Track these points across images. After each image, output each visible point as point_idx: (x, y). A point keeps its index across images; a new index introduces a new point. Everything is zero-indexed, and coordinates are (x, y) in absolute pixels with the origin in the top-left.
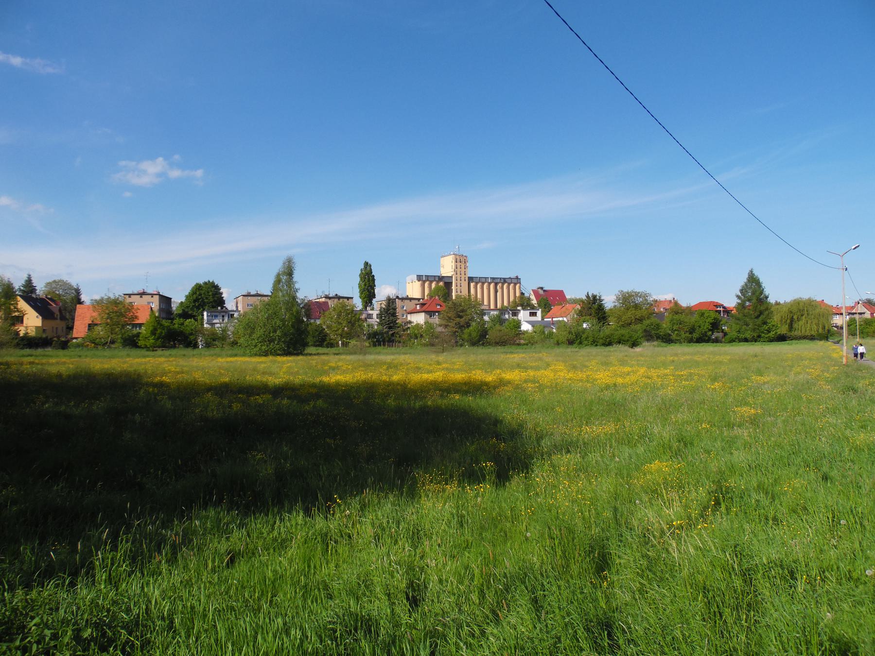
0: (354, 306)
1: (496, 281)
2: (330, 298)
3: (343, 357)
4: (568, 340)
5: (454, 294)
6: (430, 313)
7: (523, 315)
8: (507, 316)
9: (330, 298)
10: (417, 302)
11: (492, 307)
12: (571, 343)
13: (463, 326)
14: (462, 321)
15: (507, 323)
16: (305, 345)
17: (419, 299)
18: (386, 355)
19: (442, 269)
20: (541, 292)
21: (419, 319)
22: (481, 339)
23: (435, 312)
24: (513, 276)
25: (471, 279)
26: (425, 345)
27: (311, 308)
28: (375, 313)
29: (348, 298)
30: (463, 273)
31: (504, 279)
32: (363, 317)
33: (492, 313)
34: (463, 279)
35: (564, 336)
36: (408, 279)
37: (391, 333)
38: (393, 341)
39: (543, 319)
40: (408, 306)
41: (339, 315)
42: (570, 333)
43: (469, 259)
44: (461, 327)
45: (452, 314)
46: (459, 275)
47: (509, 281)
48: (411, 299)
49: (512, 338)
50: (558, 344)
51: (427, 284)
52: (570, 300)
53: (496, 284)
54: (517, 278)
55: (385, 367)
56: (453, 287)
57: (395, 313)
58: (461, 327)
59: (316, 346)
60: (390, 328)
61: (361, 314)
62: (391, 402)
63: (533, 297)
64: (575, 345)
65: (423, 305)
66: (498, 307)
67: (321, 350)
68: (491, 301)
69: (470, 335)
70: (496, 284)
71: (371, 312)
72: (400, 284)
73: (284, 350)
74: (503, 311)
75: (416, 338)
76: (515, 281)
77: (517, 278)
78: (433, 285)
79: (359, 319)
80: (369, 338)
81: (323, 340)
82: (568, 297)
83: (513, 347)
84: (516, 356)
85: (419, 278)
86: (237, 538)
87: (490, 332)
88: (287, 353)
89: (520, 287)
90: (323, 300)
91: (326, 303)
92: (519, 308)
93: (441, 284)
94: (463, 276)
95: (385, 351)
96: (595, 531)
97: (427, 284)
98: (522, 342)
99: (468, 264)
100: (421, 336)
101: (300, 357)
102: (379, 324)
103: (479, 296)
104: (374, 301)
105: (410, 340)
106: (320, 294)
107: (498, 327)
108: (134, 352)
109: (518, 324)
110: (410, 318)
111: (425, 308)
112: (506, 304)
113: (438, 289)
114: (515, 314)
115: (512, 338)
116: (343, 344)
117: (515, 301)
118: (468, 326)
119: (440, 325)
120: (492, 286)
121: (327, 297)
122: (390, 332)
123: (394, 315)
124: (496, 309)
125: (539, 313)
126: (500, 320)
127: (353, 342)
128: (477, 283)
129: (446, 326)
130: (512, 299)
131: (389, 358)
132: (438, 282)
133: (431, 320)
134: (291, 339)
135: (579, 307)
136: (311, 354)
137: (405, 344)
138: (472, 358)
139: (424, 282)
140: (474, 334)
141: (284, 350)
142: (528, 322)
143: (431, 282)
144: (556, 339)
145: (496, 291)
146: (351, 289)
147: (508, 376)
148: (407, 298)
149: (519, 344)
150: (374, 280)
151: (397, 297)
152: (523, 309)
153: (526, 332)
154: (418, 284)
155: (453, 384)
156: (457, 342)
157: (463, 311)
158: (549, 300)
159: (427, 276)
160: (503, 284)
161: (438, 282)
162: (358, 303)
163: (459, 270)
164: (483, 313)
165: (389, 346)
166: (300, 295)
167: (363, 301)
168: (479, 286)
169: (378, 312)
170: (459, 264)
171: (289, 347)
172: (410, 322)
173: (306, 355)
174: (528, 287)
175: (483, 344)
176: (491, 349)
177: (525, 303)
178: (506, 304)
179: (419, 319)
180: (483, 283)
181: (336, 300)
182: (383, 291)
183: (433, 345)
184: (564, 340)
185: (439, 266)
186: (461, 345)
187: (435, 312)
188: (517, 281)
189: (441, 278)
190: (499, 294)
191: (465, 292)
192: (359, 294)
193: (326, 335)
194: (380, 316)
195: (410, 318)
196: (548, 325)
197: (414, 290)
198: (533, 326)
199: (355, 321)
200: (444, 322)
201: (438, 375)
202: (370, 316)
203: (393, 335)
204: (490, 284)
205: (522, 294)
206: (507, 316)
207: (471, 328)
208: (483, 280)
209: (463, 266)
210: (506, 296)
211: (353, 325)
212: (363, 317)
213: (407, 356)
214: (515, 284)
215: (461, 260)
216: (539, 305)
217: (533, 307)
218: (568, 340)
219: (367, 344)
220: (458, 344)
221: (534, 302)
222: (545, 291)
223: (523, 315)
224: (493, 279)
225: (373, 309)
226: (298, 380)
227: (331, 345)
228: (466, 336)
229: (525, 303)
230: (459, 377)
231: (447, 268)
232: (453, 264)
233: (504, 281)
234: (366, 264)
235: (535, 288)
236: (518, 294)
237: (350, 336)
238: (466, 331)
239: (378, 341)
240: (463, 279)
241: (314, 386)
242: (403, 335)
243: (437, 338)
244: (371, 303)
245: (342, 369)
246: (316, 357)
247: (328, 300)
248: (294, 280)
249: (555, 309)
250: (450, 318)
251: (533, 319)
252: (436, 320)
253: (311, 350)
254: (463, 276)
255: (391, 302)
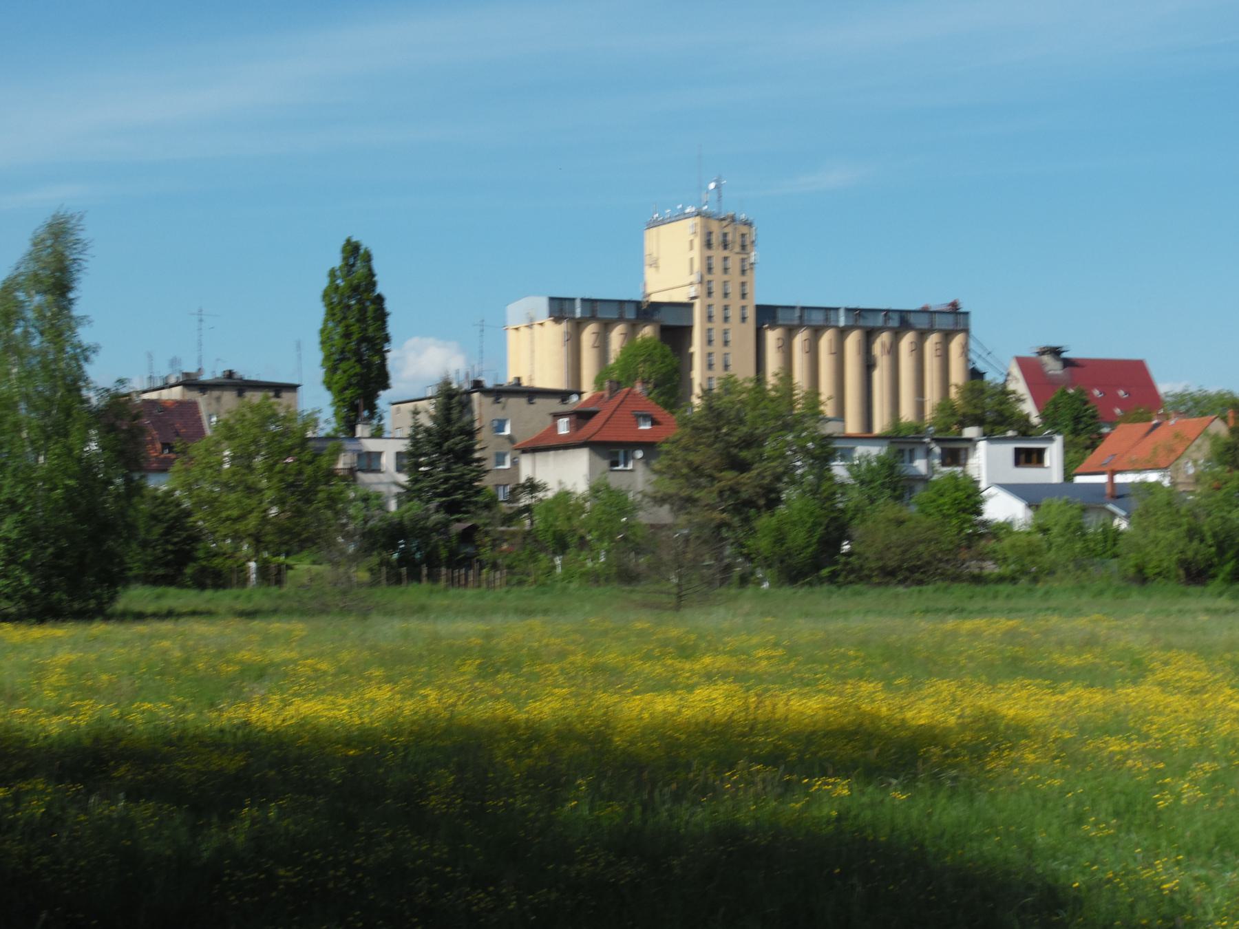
0: (878, 458)
1: (868, 324)
2: (204, 387)
3: (276, 626)
4: (1185, 564)
5: (697, 375)
6: (611, 451)
7: (988, 461)
8: (920, 465)
9: (204, 387)
10: (555, 405)
11: (852, 425)
12: (1196, 574)
13: (749, 503)
14: (748, 482)
15: (921, 493)
16: (116, 579)
17: (563, 395)
18: (454, 620)
19: (649, 273)
20: (1053, 367)
21: (568, 473)
22: (820, 559)
23: (631, 446)
24: (937, 301)
25: (767, 315)
26: (595, 578)
27: (125, 421)
28: (389, 449)
29: (279, 389)
30: (734, 290)
31: (903, 315)
32: (342, 463)
33: (861, 450)
34: (734, 313)
35: (1165, 545)
36: (516, 311)
37: (457, 528)
38: (467, 562)
39: (1068, 476)
40: (519, 421)
41: (243, 459)
42: (1193, 533)
43: (759, 233)
44: (744, 507)
45: (704, 456)
46: (717, 300)
47: (922, 321)
48: (533, 394)
49: (948, 553)
50: (1141, 578)
51: (588, 335)
52: (1181, 399)
53: (869, 335)
54: (954, 310)
55: (470, 667)
56: (697, 347)
57: (469, 450)
58: (744, 507)
59: (156, 581)
60: (452, 508)
61: (338, 451)
62: (576, 807)
63: (1019, 386)
64: (1215, 586)
65: (582, 417)
66: (878, 429)
67: (176, 598)
68: (863, 401)
69: (780, 539)
70: (869, 335)
71: (371, 445)
72: (489, 334)
73: (28, 598)
74: (903, 440)
75: (561, 545)
76: (946, 322)
77: (954, 310)
78: (616, 337)
79: (331, 474)
80: (366, 551)
81: (183, 560)
82: (1166, 387)
83: (959, 590)
84: (983, 626)
85: (560, 309)
86: (1027, 682)
87: (857, 530)
88: (42, 611)
89: (966, 349)
90: (176, 393)
91: (187, 410)
92: (970, 432)
93: (648, 331)
94: (735, 302)
95: (439, 601)
96: (1228, 669)
97: (588, 335)
98: (990, 568)
99: (753, 256)
100: (583, 543)
101: (98, 628)
102: (409, 494)
103: (826, 387)
104: (384, 399)
105: (533, 557)
106: (163, 370)
107: (887, 509)
108: (822, 599)
109: (971, 499)
110: (529, 468)
111: (590, 429)
112: (907, 413)
113: (631, 352)
114: (955, 454)
115: (948, 553)
116: (263, 571)
117: (945, 406)
118: (772, 501)
119: (660, 500)
120: (852, 342)
121: (190, 382)
122: (451, 522)
123: (465, 455)
124: (867, 435)
125: (1054, 453)
126: (891, 481)
127: (303, 567)
128: (791, 331)
129: (684, 503)
130: (932, 396)
131: (467, 629)
132: (634, 326)
133: (616, 480)
134: (59, 554)
135: (1220, 428)
136: (140, 617)
137: (516, 575)
138: (805, 630)
139: (578, 325)
140: (797, 537)
141: (28, 598)
142: (1016, 490)
143: (607, 326)
144: (1133, 559)
145: (868, 365)
146: (290, 351)
147: (1018, 703)
148: (518, 391)
149: (978, 579)
150: (381, 316)
151: (478, 385)
152: (989, 436)
153: (1004, 529)
154: (552, 334)
155: (794, 737)
156: (728, 568)
157: (751, 442)
158: (1087, 400)
159: (589, 303)
160: (897, 334)
161: (634, 326)
162: (317, 403)
163: (717, 277)
164: (825, 451)
165: (452, 582)
166: (101, 376)
167: (339, 402)
168: (799, 340)
169: (403, 446)
170: (718, 253)
171: (48, 589)
172: (532, 487)
173: (126, 616)
174: (1001, 351)
175: (832, 578)
176: (872, 596)
177: (986, 410)
178: (907, 413)
179: (568, 473)
180: (817, 331)
181: (229, 398)
182: (420, 363)
183: (628, 577)
184: (1170, 561)
185: (637, 261)
186: (744, 580)
187: (631, 446)
188: (952, 321)
189: (646, 311)
190: (880, 377)
191: (744, 370)
192: (320, 373)
193: (195, 538)
194: (407, 461)
195: (529, 468)
196: (1095, 499)
197: (535, 355)
198: (1032, 505)
199: (315, 481)
200: (671, 487)
201: (710, 701)
202: (370, 462)
203: (468, 536)
204: (842, 333)
205: (975, 375)
206: (920, 465)
207: (782, 509)
208: (817, 319)
209: (734, 263)
210: (911, 387)
211: (307, 496)
212: (342, 463)
213: (536, 622)
214: (948, 336)
215: (726, 238)
216: (1052, 421)
217: (1025, 429)
218: (1185, 564)
219: (363, 575)
220: (731, 578)
221: (1029, 408)
222: (1068, 363)
223: (988, 461)
224: (857, 314)
225: (378, 434)
226: (150, 713)
227: (216, 578)
228: (763, 544)
229: (986, 410)
230: (806, 706)
231: (670, 267)
232: (696, 254)
233: (902, 322)
234: (353, 251)
235: (1028, 352)
236: (957, 376)
237: (295, 537)
238: (765, 521)
239: (405, 560)
240: (734, 313)
241: (217, 743)
242: (501, 538)
243: (638, 550)
244: (372, 408)
245: (319, 674)
246: (166, 626)
247: (194, 395)
248: (77, 311)
249: (1118, 438)
250: (696, 470)
251: (1029, 475)
252: (636, 477)
253: (136, 596)
254: (735, 302)
255: (453, 401)
